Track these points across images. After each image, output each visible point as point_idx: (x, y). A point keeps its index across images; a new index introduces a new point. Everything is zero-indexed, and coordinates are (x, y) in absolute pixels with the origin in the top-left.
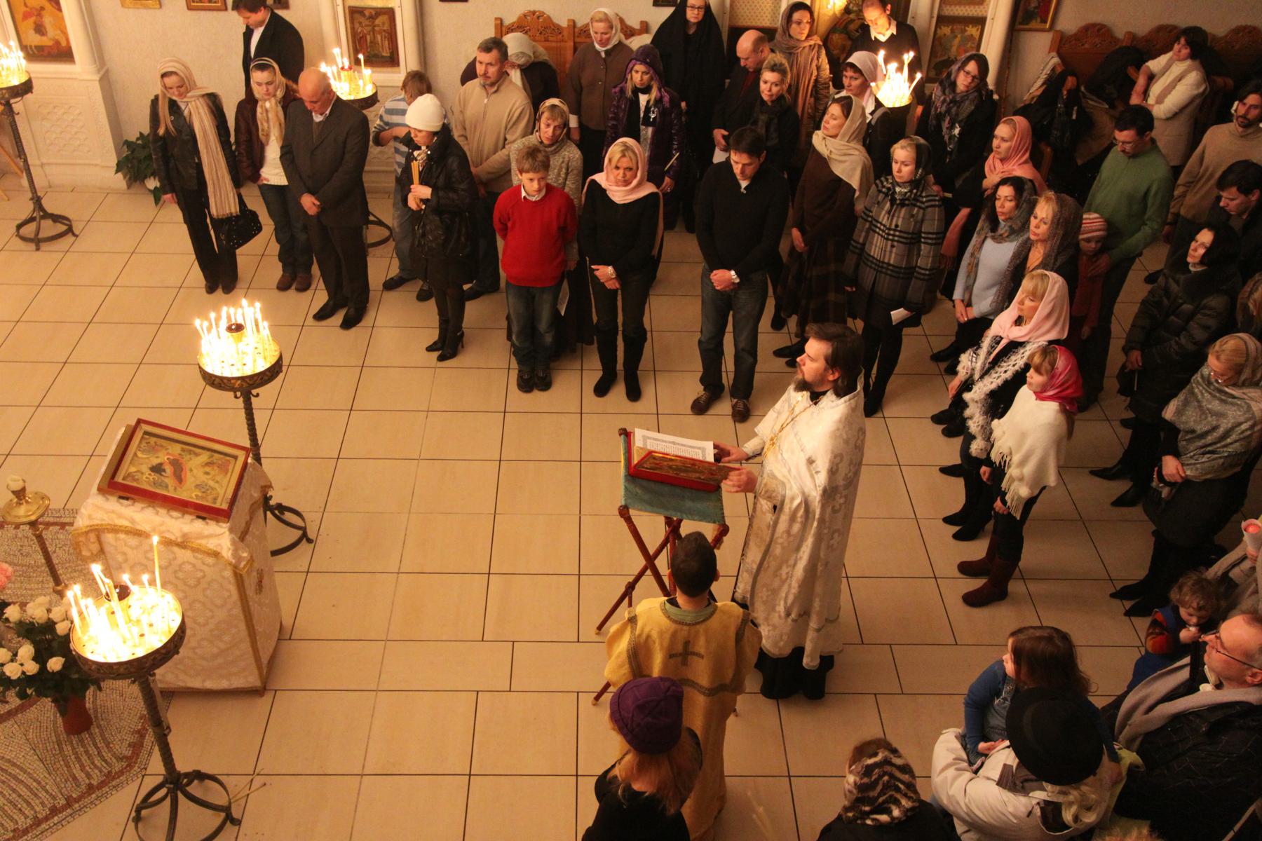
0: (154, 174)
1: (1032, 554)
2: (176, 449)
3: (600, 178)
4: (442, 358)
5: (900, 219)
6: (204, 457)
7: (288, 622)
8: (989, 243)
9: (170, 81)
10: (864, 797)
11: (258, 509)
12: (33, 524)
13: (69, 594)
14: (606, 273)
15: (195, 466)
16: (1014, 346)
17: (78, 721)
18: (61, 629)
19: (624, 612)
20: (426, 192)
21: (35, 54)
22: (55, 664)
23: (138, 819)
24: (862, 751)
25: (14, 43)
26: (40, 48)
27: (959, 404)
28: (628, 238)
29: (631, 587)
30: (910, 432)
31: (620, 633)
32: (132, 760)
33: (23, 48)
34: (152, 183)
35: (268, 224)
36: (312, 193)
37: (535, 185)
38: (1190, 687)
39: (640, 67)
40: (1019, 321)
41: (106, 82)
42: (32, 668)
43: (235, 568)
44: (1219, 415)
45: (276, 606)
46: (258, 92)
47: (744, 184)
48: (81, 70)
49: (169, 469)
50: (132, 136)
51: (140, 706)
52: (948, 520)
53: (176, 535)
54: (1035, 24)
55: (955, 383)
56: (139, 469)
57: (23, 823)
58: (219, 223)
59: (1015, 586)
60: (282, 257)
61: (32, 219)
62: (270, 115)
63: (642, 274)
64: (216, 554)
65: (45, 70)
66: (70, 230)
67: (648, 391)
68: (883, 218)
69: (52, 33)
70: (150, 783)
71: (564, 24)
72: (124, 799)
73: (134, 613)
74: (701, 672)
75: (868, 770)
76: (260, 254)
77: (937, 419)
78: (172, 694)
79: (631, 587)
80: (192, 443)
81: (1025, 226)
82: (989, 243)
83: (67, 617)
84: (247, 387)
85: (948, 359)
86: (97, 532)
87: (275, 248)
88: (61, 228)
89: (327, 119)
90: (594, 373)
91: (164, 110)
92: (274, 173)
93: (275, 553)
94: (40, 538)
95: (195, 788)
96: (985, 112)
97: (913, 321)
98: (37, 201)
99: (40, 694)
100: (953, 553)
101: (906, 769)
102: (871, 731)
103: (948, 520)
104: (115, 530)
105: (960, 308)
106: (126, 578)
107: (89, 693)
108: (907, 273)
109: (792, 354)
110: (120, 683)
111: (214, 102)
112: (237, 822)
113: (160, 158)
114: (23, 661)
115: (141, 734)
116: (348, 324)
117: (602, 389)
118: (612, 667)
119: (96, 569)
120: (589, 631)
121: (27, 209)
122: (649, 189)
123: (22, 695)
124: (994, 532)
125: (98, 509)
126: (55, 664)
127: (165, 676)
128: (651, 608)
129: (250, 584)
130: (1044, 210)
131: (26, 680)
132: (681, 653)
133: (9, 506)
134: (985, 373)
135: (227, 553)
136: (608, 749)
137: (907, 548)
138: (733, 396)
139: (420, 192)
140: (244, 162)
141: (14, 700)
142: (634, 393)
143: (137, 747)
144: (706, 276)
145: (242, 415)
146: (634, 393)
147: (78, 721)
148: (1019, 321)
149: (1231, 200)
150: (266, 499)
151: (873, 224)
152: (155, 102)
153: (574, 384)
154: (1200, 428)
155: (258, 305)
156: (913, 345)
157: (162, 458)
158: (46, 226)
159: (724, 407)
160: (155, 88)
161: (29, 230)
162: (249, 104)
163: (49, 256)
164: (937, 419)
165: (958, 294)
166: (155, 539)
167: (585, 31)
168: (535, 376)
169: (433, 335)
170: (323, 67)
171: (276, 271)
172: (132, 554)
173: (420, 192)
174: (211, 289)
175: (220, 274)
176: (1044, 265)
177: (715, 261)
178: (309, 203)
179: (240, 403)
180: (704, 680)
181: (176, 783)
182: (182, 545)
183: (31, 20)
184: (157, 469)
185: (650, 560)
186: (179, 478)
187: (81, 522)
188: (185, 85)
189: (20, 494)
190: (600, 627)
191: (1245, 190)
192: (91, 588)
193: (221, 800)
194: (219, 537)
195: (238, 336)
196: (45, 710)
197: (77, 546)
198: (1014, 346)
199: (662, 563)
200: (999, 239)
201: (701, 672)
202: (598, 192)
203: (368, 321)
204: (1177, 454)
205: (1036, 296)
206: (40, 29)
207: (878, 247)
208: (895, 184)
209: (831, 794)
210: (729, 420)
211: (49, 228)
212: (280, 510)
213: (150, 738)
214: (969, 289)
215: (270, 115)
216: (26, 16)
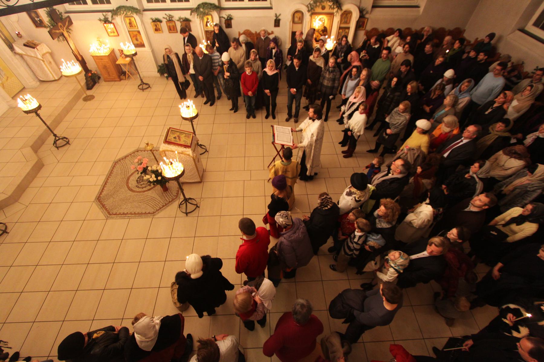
0: (166, 73)
1: (358, 149)
2: (178, 134)
3: (265, 70)
4: (235, 112)
5: (331, 76)
6: (184, 135)
7: (205, 168)
8: (350, 81)
9: (167, 50)
10: (322, 204)
11: (196, 145)
12: (151, 150)
13: (160, 164)
14: (267, 91)
15: (182, 136)
16: (354, 104)
17: (166, 189)
18: (160, 171)
19: (273, 164)
20: (228, 74)
21: (137, 46)
22: (159, 178)
23: (180, 207)
24: (321, 195)
25: (132, 43)
26: (138, 44)
27: (342, 118)
28: (272, 83)
29: (274, 159)
30: (332, 123)
31: (272, 168)
32: (177, 196)
33: (134, 44)
34: (166, 75)
35: (192, 83)
36: (201, 75)
37: (249, 71)
38: (387, 175)
39: (272, 43)
40: (355, 98)
41: (153, 51)
42: (155, 179)
43: (193, 158)
44: (399, 120)
45: (202, 165)
46: (187, 52)
47: (297, 68)
48: (147, 49)
49: (177, 138)
50: (160, 64)
51: (177, 186)
52: (340, 143)
53: (180, 151)
54: (361, 28)
55: (341, 113)
56: (171, 138)
57: (158, 208)
58: (182, 84)
59: (354, 155)
60: (195, 90)
61: (141, 85)
62: (190, 57)
63: (275, 92)
64: (189, 155)
65: (139, 50)
66: (149, 87)
67: (277, 117)
68: (327, 76)
69: (139, 40)
70: (181, 200)
71: (254, 32)
72: (176, 204)
73: (174, 167)
74: (289, 175)
75: (322, 200)
76: (191, 90)
77: (338, 121)
78: (183, 183)
79: (274, 159)
80: (182, 132)
81: (359, 76)
82: (350, 81)
83: (160, 169)
84: (191, 120)
85: (339, 107)
86: (164, 151)
87: (194, 88)
88: (147, 86)
89: (203, 58)
90: (265, 114)
91: (166, 57)
92: (192, 71)
93: (201, 154)
94: (153, 153)
95: (190, 201)
96: (349, 49)
97: (333, 98)
98: (142, 80)
99: (157, 184)
100: (340, 149)
101: (330, 198)
102: (324, 190)
103: (340, 143)
104: (168, 151)
105: (343, 96)
106: (171, 160)
107: (167, 184)
108: (333, 88)
109: (307, 108)
110: (172, 181)
111: (177, 55)
112: (199, 207)
113: (166, 69)
114: (153, 178)
115: (178, 191)
116: (211, 105)
117: (267, 117)
118: (271, 175)
119: (165, 158)
120: (266, 168)
121: (140, 82)
122: (275, 72)
123: (154, 184)
124: (350, 144)
125: (164, 147)
126: (159, 178)
127: (182, 180)
128: (278, 163)
129: (197, 161)
130: (364, 73)
131: (154, 181)
132: (285, 171)
133: (146, 147)
134: (348, 110)
135: (191, 154)
136: (271, 190)
137: (332, 150)
138: (294, 117)
139: (227, 74)
140: (185, 68)
141: (152, 186)
142: (274, 118)
143: (178, 194)
144: (289, 91)
145: (191, 125)
146: (274, 118)
147: (166, 189)
148: (355, 98)
149: (403, 69)
150: (198, 143)
151: (324, 78)
152: (164, 56)
153: (261, 116)
154: (395, 123)
155: (192, 101)
156: (333, 104)
157: (175, 135)
158: (144, 86)
159: (293, 120)
160: (163, 52)
161: (141, 87)
162: (185, 55)
163: (146, 92)
164: (338, 121)
165: (343, 93)
166: (176, 152)
167: (259, 34)
168: (251, 114)
169: (231, 107)
170: (201, 46)
171: (194, 93)
172: (172, 156)
173: (227, 74)
174: (181, 98)
175: (183, 95)
176: (362, 85)
177: (290, 86)
178: (201, 78)
179: (190, 123)
180: (290, 176)
181: (186, 200)
182: (182, 153)
183: (135, 38)
184: (175, 138)
185: (278, 152)
186: (180, 140)
187: (161, 150)
188: (170, 51)
189: (148, 144)
190: (268, 167)
191: (407, 66)
192: (165, 162)
193: (195, 203)
194: (189, 151)
195: (189, 108)
196: (159, 187)
197: (160, 154)
198: (354, 104)
199: (281, 153)
200: (352, 80)
201: (289, 175)
202: (265, 73)
203: (215, 104)
204: (390, 128)
205: (359, 92)
206: (137, 40)
207: (326, 83)
208: (329, 67)
209: (316, 202)
210: (294, 123)
211: (145, 86)
212: (201, 145)
213: (180, 192)
214: (345, 91)
215: (190, 57)
216: (134, 37)
